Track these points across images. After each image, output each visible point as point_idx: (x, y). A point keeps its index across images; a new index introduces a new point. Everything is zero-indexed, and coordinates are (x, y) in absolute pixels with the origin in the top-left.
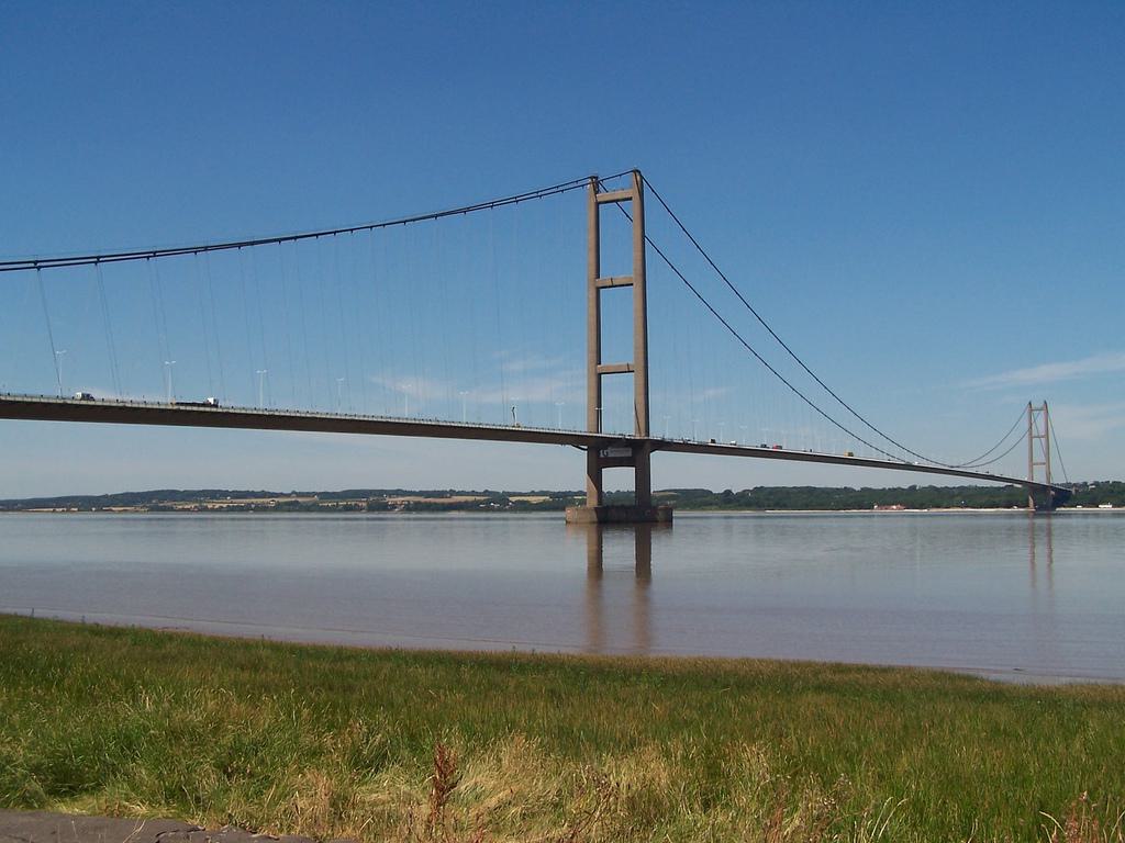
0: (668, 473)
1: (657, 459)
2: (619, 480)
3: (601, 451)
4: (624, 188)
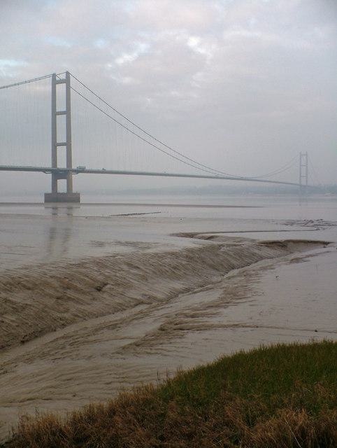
1: (75, 177)
2: (62, 185)
3: (57, 174)
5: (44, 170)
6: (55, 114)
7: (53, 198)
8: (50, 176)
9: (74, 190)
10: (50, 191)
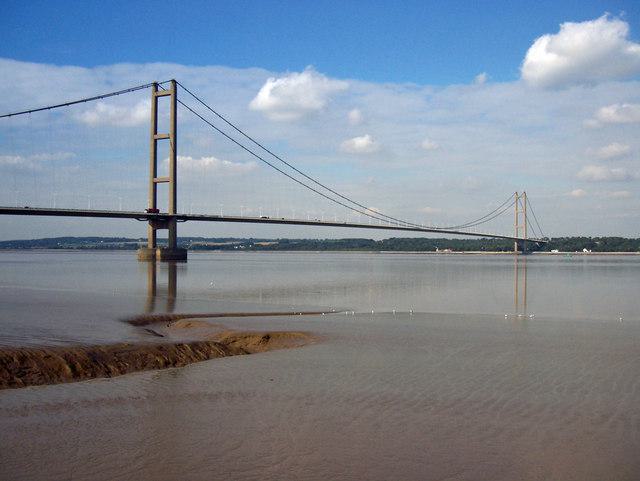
0: (184, 230)
1: (180, 225)
2: (163, 234)
3: (157, 220)
4: (169, 86)
5: (138, 217)
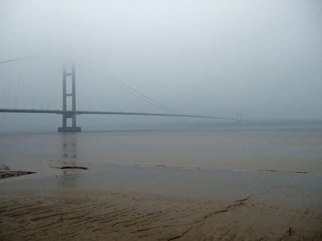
1: (77, 116)
3: (67, 114)
5: (57, 112)
6: (65, 96)
7: (64, 130)
8: (61, 116)
9: (77, 126)
10: (61, 125)
